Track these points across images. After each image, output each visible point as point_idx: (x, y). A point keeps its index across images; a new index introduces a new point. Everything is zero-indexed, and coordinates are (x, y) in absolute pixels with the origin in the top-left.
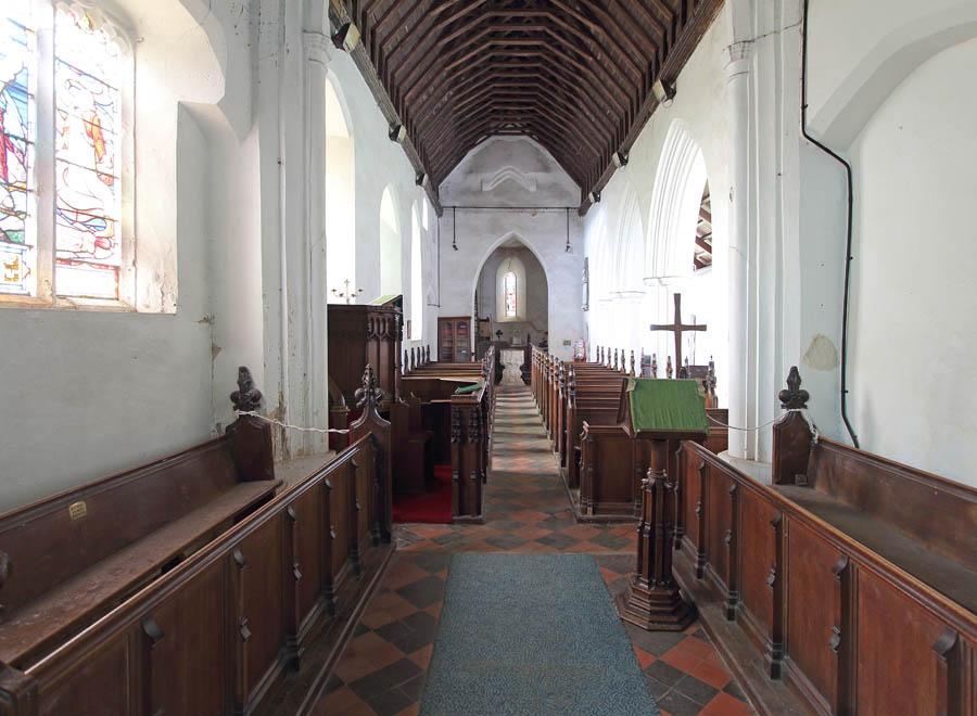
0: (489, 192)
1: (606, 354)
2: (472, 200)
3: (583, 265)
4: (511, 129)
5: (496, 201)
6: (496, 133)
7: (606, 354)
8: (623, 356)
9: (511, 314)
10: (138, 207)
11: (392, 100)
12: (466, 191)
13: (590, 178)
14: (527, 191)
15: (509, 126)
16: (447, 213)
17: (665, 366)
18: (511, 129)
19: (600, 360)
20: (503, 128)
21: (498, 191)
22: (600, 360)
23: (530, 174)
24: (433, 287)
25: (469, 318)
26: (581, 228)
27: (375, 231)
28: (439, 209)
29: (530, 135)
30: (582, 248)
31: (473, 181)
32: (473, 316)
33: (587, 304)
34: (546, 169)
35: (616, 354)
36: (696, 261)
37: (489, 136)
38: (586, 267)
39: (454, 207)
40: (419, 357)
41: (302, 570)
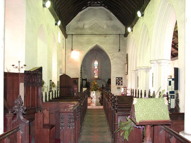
0: (87, 28)
1: (137, 92)
2: (79, 32)
3: (126, 56)
4: (96, 4)
5: (90, 32)
6: (90, 6)
7: (137, 92)
8: (145, 93)
9: (96, 77)
10: (5, 55)
11: (55, 11)
12: (77, 28)
13: (128, 19)
14: (103, 28)
15: (96, 3)
16: (69, 38)
17: (144, 93)
18: (96, 4)
19: (132, 95)
20: (93, 4)
21: (91, 28)
22: (132, 95)
23: (95, 100)
24: (62, 66)
25: (78, 78)
26: (125, 44)
27: (55, 55)
28: (66, 36)
29: (104, 6)
30: (125, 49)
31: (80, 24)
32: (79, 78)
33: (127, 72)
34: (111, 19)
35: (139, 92)
36: (172, 55)
37: (87, 7)
38: (127, 58)
39: (72, 35)
40: (55, 94)
41: (83, 104)
